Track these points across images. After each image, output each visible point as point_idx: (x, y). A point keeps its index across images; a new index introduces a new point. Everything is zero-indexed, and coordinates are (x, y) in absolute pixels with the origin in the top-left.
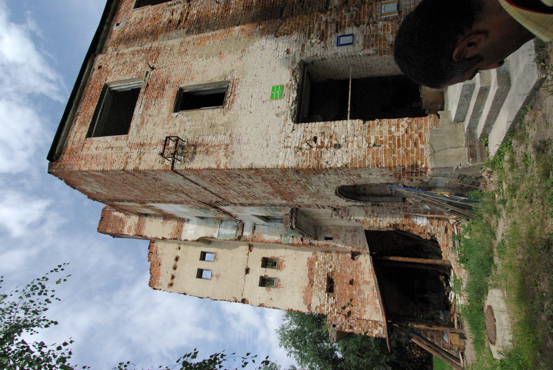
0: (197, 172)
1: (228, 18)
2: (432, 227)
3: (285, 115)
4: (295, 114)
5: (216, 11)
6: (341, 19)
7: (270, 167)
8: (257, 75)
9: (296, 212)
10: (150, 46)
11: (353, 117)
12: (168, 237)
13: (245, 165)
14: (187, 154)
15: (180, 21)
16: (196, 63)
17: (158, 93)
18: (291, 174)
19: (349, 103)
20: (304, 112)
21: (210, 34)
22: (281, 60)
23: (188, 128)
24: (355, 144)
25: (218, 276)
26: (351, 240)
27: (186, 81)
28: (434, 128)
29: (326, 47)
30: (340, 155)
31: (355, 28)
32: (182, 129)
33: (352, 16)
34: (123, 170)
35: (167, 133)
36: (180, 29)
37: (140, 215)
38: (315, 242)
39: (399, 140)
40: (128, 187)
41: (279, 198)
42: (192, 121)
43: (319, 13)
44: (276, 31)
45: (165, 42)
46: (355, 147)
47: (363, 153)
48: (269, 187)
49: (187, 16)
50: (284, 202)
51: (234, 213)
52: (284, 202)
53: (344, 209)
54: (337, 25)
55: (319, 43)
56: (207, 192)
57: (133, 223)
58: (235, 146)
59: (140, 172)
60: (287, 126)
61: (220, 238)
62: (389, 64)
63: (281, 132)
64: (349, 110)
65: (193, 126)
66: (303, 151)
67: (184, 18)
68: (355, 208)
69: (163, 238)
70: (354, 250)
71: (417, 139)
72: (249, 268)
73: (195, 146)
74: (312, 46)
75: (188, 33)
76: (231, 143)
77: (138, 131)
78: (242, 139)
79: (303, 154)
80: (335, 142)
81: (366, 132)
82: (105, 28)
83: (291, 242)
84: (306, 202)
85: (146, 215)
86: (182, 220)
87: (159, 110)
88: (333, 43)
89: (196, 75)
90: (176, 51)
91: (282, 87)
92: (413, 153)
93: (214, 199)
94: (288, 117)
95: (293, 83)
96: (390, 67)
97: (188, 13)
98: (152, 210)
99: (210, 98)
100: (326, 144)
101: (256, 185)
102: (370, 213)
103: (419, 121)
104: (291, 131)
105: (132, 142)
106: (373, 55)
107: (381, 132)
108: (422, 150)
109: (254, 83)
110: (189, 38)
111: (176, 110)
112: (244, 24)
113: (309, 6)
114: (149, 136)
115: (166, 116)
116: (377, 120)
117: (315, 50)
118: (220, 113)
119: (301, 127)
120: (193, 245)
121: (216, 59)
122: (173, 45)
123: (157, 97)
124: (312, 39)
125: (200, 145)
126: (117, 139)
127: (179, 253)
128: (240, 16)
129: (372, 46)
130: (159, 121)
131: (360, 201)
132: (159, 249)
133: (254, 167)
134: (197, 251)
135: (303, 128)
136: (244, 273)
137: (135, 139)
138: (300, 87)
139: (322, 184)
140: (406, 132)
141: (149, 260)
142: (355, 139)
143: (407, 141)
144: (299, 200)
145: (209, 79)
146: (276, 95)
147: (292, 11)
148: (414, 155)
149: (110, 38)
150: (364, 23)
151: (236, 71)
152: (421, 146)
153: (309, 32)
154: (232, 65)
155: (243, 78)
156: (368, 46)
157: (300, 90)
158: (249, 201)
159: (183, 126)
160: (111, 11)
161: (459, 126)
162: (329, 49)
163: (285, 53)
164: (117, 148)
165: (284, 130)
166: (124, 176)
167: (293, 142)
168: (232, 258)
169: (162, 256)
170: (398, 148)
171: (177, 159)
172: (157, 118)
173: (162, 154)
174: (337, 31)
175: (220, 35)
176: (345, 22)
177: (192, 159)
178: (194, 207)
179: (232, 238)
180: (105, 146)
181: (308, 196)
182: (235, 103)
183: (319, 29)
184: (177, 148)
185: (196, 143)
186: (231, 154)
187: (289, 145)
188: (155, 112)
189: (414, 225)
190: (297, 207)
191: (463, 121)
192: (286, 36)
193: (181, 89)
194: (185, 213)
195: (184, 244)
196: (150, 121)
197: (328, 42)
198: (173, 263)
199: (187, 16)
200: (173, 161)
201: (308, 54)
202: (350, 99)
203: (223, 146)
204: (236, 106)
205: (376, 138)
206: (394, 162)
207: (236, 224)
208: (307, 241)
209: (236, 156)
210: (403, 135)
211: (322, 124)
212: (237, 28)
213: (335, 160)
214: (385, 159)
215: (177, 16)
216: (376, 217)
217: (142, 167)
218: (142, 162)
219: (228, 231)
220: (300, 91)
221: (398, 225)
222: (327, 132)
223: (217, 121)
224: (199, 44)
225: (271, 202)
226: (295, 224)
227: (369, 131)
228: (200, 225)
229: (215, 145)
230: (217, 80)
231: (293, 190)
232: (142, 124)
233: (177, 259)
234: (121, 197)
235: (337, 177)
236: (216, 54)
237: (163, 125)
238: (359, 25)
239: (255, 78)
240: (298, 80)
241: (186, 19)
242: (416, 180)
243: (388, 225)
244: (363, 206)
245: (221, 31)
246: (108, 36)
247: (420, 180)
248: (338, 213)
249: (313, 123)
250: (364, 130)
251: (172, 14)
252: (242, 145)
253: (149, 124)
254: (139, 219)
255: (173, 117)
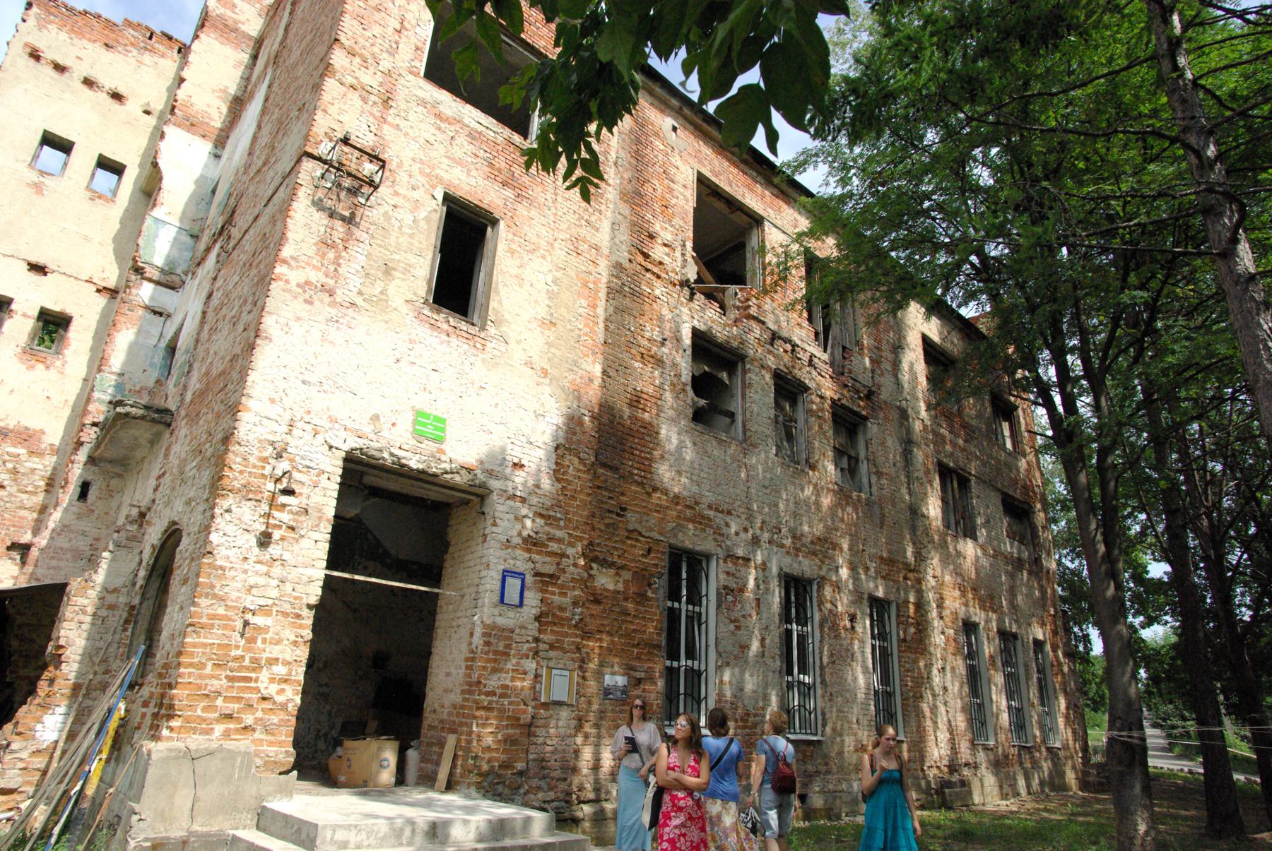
0: (285, 210)
1: (626, 356)
2: (24, 755)
3: (372, 436)
4: (368, 456)
5: (647, 335)
6: (562, 587)
7: (250, 379)
8: (482, 392)
9: (161, 418)
10: (610, 181)
11: (329, 583)
12: (181, 94)
13: (269, 322)
14: (334, 197)
15: (646, 256)
16: (545, 269)
17: (500, 171)
18: (224, 424)
19: (373, 580)
20: (363, 477)
21: (600, 311)
22: (503, 450)
23: (399, 214)
24: (262, 581)
25: (38, 188)
26: (67, 545)
27: (510, 236)
28: (259, 762)
29: (507, 548)
30: (238, 544)
31: (534, 611)
32: (399, 201)
33: (562, 609)
34: (337, 40)
35: (400, 165)
36: (630, 253)
37: (259, 43)
38: (82, 456)
39: (249, 679)
40: (309, 38)
41: (198, 386)
42: (411, 228)
43: (585, 543)
44: (569, 450)
45: (609, 214)
46: (252, 581)
47: (234, 595)
48: (221, 368)
49: (654, 273)
50: (188, 398)
51: (201, 272)
52: (188, 398)
53: (137, 539)
54: (551, 576)
55: (520, 534)
56: (251, 219)
57: (241, 18)
58: (323, 308)
59: (322, 76)
60: (343, 434)
61: (149, 221)
62: (448, 674)
63: (333, 420)
64: (357, 577)
65: (400, 228)
66: (271, 461)
67: (650, 266)
68: (134, 564)
69: (182, 80)
70: (34, 553)
71: (239, 720)
72: (45, 274)
73: (350, 221)
74: (516, 518)
75: (618, 266)
76: (334, 302)
77: (423, 103)
78: (338, 329)
79: (265, 460)
80: (277, 535)
81: (287, 608)
82: (675, 102)
83: (96, 395)
84: (176, 448)
85: (255, 57)
86: (221, 141)
87: (459, 162)
88: (512, 562)
89: (517, 262)
90: (584, 232)
91: (439, 441)
92: (204, 709)
93: (235, 233)
94: (367, 442)
95: (443, 466)
96: (442, 676)
97: (659, 277)
98: (259, 78)
99: (457, 281)
100: (276, 514)
101: (231, 338)
102: (111, 599)
103: (284, 730)
104: (329, 441)
105: (401, 81)
106: (470, 644)
107: (278, 642)
108: (209, 732)
109: (464, 381)
110: (604, 269)
111: (448, 198)
112: (604, 386)
113: (608, 526)
114: (403, 124)
115: (442, 174)
116: (311, 636)
117: (508, 523)
118: (415, 294)
119: (334, 467)
120: (148, 149)
121: (542, 312)
122: (597, 230)
123: (491, 165)
124: (533, 521)
125: (349, 233)
126: (417, 49)
127: (133, 107)
128: (622, 381)
129: (487, 644)
130: (433, 154)
131: (149, 578)
132: (156, 59)
133: (258, 341)
134: (130, 155)
135: (329, 469)
136: (34, 260)
137: (406, 91)
138: (430, 479)
139: (192, 494)
140: (264, 699)
141: (128, 23)
142: (275, 582)
143: (239, 699)
144: (183, 432)
145: (500, 286)
146: (426, 425)
147: (606, 489)
148: (199, 712)
149: (651, 104)
150: (540, 631)
151: (503, 349)
152: (219, 729)
153: (549, 517)
154: (519, 342)
155: (484, 360)
156: (489, 635)
157: (422, 477)
158: (210, 315)
159: (407, 204)
160: (705, 126)
161: (250, 819)
162: (503, 553)
163: (516, 460)
164: (397, 43)
165: (336, 426)
166: (326, 37)
167: (301, 442)
168: (86, 239)
169: (133, 61)
170: (227, 677)
171: (327, 170)
172: (442, 152)
173: (346, 141)
174: (537, 574)
175: (592, 330)
176: (553, 593)
177: (318, 205)
178: (236, 181)
179: (141, 252)
180: (409, 16)
181: (183, 455)
182: (429, 331)
183: (550, 539)
184: (354, 182)
185: (357, 225)
186: (307, 296)
187: (295, 432)
188: (458, 153)
189: (45, 707)
190: (174, 425)
191: (258, 827)
192: (554, 467)
193: (494, 222)
194: (233, 153)
195: (155, 128)
196: (440, 136)
197: (518, 552)
198: (109, 82)
199: (654, 273)
200: (325, 162)
201: (498, 506)
202: (384, 582)
203: (332, 282)
204: (423, 332)
205: (266, 629)
206: (191, 665)
207: (179, 271)
208: (90, 435)
209: (299, 307)
210: (258, 690)
211: (331, 512)
212: (598, 370)
213: (230, 529)
214: (205, 645)
215: (658, 252)
216: (94, 615)
217: (330, 84)
218: (344, 89)
219: (160, 246)
220: (422, 476)
221: (57, 667)
222: (307, 523)
223: (397, 282)
224: (585, 285)
225: (196, 365)
226: (127, 415)
227: (285, 614)
228: (197, 182)
229: (339, 265)
230: (493, 304)
231: (201, 422)
232: (438, 116)
233: (117, 96)
234: (299, 12)
235: (196, 529)
236: (552, 315)
237: (422, 162)
238: (540, 622)
239: (477, 385)
240: (448, 476)
241: (647, 270)
242: (144, 715)
243: (62, 642)
244: (134, 584)
245: (601, 337)
246: (656, 103)
247: (140, 724)
248: (131, 523)
249: (335, 494)
250: (292, 604)
251: (665, 245)
252: (324, 327)
253: (433, 130)
254: (250, 38)
255: (434, 187)
